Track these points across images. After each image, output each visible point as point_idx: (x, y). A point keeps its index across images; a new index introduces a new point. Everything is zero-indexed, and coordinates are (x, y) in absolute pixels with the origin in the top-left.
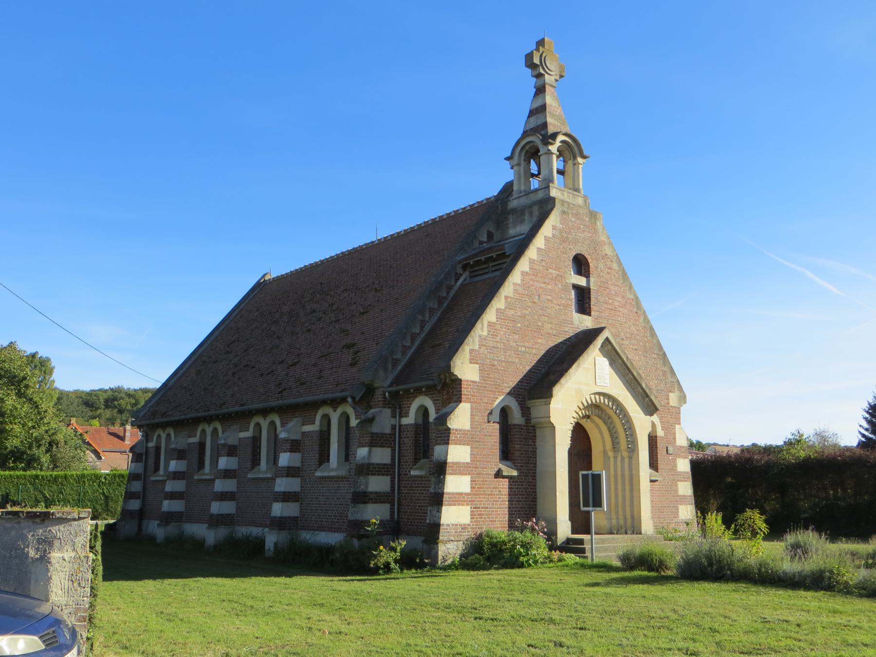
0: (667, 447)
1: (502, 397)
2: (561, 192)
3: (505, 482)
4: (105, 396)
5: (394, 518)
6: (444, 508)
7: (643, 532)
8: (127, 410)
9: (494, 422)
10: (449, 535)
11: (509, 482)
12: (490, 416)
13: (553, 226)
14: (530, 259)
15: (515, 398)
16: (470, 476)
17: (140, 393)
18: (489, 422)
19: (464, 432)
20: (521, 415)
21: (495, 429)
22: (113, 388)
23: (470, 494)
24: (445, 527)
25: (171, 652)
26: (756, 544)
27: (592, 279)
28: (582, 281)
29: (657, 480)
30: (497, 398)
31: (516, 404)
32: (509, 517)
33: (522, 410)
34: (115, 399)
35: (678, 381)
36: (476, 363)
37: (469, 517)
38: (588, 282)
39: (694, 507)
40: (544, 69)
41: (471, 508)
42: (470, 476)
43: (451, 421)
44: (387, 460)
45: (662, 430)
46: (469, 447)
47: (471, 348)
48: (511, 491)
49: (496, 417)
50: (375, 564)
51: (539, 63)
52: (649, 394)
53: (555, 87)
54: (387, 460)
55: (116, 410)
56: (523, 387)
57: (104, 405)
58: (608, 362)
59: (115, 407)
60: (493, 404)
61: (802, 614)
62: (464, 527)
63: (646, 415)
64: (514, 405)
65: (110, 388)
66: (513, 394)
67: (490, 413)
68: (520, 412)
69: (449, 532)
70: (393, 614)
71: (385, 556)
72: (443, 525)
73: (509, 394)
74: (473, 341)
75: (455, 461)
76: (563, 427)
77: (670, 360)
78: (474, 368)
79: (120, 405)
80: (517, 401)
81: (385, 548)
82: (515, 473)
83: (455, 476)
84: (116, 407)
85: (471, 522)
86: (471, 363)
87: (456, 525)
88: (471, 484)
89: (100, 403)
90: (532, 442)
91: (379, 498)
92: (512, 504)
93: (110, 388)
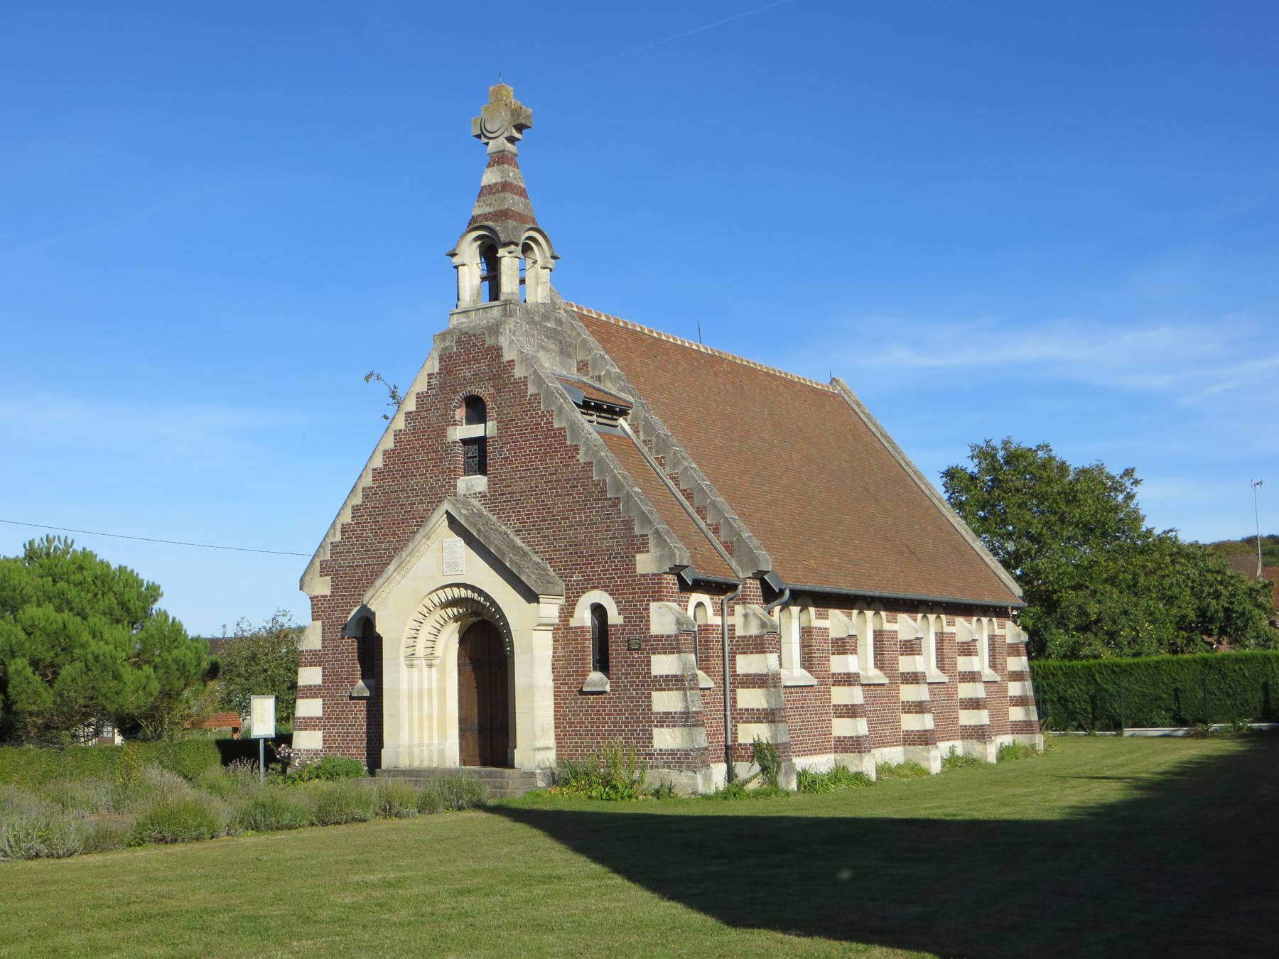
3: (362, 704)
5: (1227, 730)
19: (315, 653)
23: (322, 718)
26: (824, 783)
30: (352, 610)
32: (367, 743)
36: (327, 575)
37: (655, 735)
44: (740, 692)
49: (352, 631)
53: (494, 293)
54: (740, 692)
60: (347, 617)
70: (396, 838)
74: (324, 552)
85: (324, 747)
88: (323, 708)
91: (667, 720)
92: (370, 729)
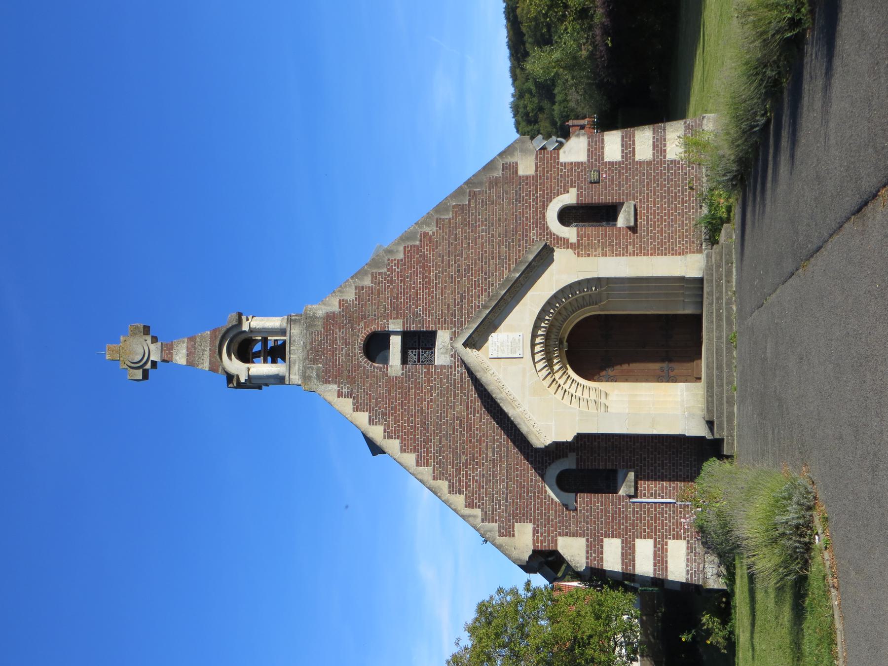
0: (591, 183)
1: (548, 488)
2: (292, 365)
4: (523, 124)
6: (671, 577)
7: (700, 276)
8: (539, 102)
9: (576, 502)
10: (698, 571)
11: (641, 480)
12: (570, 508)
13: (339, 397)
14: (385, 438)
15: (546, 468)
16: (637, 540)
17: (517, 83)
18: (576, 509)
20: (565, 459)
21: (583, 500)
22: (513, 114)
23: (655, 540)
24: (689, 576)
25: (806, 498)
27: (392, 328)
28: (396, 342)
29: (635, 206)
30: (549, 496)
31: (553, 466)
32: (680, 481)
33: (560, 457)
34: (527, 114)
35: (501, 155)
36: (513, 527)
38: (396, 333)
39: (669, 123)
40: (146, 363)
41: (670, 538)
42: (637, 540)
43: (578, 565)
45: (568, 192)
46: (605, 540)
47: (497, 534)
48: (652, 478)
50: (725, 648)
51: (141, 370)
52: (527, 264)
55: (541, 116)
56: (533, 454)
57: (534, 125)
58: (493, 334)
59: (536, 116)
61: (808, 625)
62: (690, 549)
63: (553, 260)
64: (554, 470)
65: (513, 117)
66: (543, 469)
67: (566, 506)
68: (562, 460)
69: (695, 571)
71: (717, 638)
72: (687, 579)
73: (542, 476)
74: (490, 531)
75: (620, 561)
76: (577, 418)
77: (474, 173)
78: (519, 531)
79: (533, 110)
80: (550, 464)
81: (708, 639)
82: (631, 475)
83: (636, 562)
84: (536, 113)
85: (685, 539)
86: (513, 535)
87: (688, 559)
89: (532, 130)
90: (595, 441)
93: (513, 117)
